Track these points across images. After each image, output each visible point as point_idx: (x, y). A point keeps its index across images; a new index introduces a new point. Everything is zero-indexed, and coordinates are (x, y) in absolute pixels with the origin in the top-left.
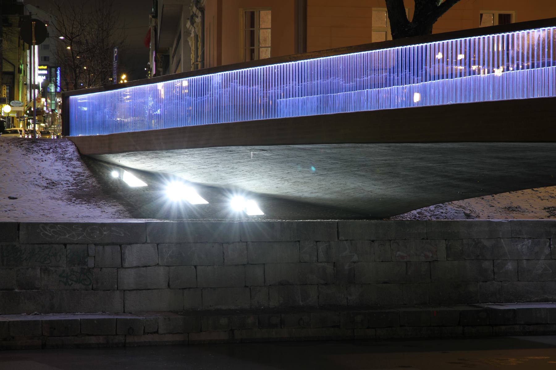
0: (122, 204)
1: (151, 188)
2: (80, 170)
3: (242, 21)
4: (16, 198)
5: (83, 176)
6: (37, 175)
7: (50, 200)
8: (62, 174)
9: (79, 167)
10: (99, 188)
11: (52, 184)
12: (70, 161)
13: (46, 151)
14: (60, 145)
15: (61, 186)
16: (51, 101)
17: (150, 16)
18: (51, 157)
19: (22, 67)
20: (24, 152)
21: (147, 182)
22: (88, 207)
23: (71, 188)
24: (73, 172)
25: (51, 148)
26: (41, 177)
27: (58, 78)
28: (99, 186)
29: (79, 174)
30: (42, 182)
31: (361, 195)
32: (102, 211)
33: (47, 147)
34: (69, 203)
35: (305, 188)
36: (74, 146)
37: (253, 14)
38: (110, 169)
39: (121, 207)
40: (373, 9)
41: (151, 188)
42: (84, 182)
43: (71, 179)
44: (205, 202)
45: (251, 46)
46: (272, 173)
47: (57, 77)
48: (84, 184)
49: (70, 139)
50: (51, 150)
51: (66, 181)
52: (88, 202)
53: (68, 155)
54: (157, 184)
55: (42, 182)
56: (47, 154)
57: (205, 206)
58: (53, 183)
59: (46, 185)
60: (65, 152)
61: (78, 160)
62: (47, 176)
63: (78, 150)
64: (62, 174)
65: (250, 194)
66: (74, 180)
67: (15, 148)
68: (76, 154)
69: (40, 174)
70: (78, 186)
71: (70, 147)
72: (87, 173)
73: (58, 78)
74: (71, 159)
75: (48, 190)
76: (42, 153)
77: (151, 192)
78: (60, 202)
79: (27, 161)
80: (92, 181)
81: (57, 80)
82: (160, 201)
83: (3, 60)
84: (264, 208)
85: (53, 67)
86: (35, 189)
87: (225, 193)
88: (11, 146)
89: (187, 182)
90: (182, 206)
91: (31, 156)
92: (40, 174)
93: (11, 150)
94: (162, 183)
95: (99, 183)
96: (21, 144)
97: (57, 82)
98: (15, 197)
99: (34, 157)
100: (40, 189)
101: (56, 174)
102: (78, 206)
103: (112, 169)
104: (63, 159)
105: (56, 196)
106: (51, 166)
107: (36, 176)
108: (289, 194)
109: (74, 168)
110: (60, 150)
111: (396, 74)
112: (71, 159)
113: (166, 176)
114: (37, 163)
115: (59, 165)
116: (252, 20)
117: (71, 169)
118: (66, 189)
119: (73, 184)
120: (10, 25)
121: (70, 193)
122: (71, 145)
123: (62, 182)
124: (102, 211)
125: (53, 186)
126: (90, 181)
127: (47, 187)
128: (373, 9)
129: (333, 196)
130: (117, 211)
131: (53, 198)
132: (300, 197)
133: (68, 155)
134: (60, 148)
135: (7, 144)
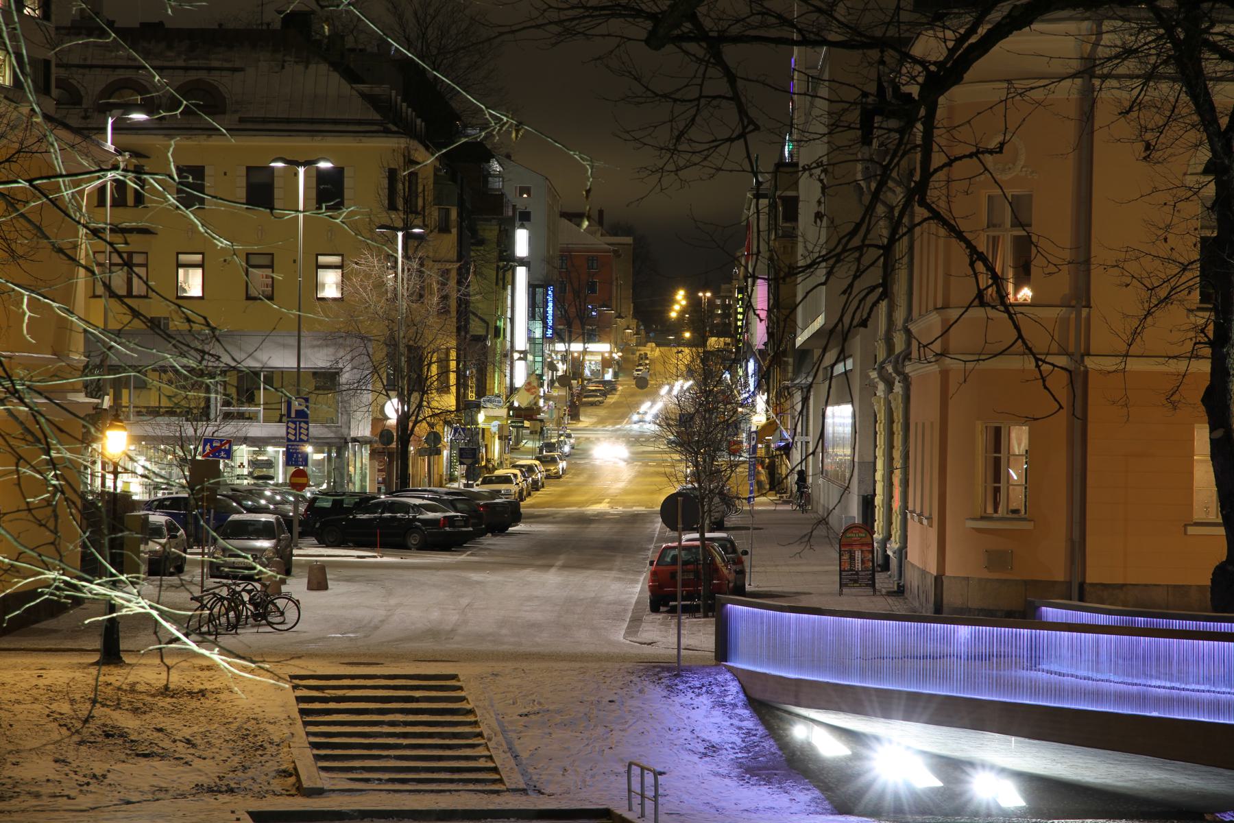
0: (817, 787)
1: (856, 757)
2: (749, 724)
3: (981, 441)
4: (664, 773)
5: (755, 735)
6: (689, 733)
7: (712, 778)
8: (725, 731)
9: (750, 723)
10: (781, 756)
11: (712, 749)
12: (732, 709)
13: (696, 690)
14: (716, 679)
15: (724, 751)
16: (534, 356)
17: (749, 195)
18: (705, 702)
19: (500, 324)
20: (665, 693)
21: (851, 748)
22: (769, 791)
23: (740, 755)
24: (740, 728)
25: (703, 685)
26: (694, 736)
27: (550, 310)
28: (780, 753)
29: (749, 733)
30: (697, 745)
31: (1171, 787)
32: (791, 800)
33: (698, 684)
34: (741, 783)
35: (1087, 773)
36: (736, 683)
37: (998, 431)
38: (791, 723)
39: (817, 793)
40: (1196, 425)
41: (856, 757)
42: (757, 746)
43: (739, 741)
44: (938, 783)
45: (995, 482)
46: (1040, 754)
47: (547, 306)
48: (757, 749)
49: (731, 670)
50: (704, 689)
51: (732, 743)
52: (769, 782)
53: (731, 697)
54: (865, 752)
55: (697, 745)
56: (698, 695)
57: (938, 789)
58: (713, 747)
59: (704, 751)
60: (724, 693)
61: (745, 706)
62: (704, 736)
63: (744, 689)
64: (725, 731)
65: (1003, 771)
66: (743, 741)
67: (651, 686)
68: (741, 696)
69: (692, 731)
70: (749, 752)
71: (731, 683)
72: (761, 730)
73: (550, 310)
74: (735, 706)
75: (707, 759)
76: (690, 695)
77: (858, 763)
78: (727, 781)
79: (671, 708)
80: (769, 745)
81: (547, 312)
82: (868, 777)
83: (472, 317)
84: (1027, 794)
85: (539, 286)
86: (688, 758)
87: (965, 768)
88: (645, 683)
89: (908, 748)
90: (903, 791)
91: (676, 699)
92: (692, 731)
93: (646, 689)
94: (870, 748)
95: (780, 749)
96: (660, 679)
97: (547, 318)
98: (662, 770)
99: (681, 701)
100: (695, 758)
101: (715, 731)
102: (755, 788)
103: (795, 722)
104: (723, 705)
105: (721, 771)
106: (706, 717)
107: (687, 734)
108: (1063, 776)
109: (741, 720)
110: (716, 689)
111: (1216, 674)
112: (735, 706)
113: (877, 738)
114: (685, 713)
115: (718, 716)
116: (997, 439)
117: (736, 722)
118: (733, 756)
119: (742, 749)
120: (481, 242)
121: (740, 765)
122: (733, 680)
123: (726, 746)
124: (792, 800)
125: (714, 752)
126: (766, 744)
127: (705, 755)
128: (1196, 425)
129: (1129, 784)
130: (813, 800)
131: (717, 774)
132: (1079, 781)
133: (731, 697)
134: (717, 685)
135: (638, 679)
